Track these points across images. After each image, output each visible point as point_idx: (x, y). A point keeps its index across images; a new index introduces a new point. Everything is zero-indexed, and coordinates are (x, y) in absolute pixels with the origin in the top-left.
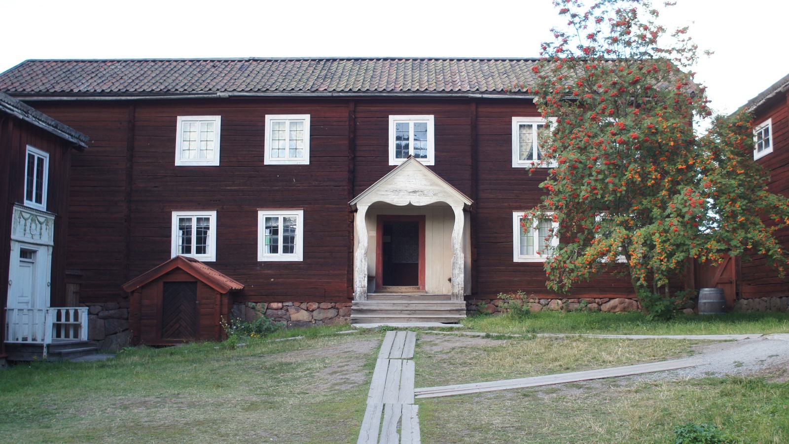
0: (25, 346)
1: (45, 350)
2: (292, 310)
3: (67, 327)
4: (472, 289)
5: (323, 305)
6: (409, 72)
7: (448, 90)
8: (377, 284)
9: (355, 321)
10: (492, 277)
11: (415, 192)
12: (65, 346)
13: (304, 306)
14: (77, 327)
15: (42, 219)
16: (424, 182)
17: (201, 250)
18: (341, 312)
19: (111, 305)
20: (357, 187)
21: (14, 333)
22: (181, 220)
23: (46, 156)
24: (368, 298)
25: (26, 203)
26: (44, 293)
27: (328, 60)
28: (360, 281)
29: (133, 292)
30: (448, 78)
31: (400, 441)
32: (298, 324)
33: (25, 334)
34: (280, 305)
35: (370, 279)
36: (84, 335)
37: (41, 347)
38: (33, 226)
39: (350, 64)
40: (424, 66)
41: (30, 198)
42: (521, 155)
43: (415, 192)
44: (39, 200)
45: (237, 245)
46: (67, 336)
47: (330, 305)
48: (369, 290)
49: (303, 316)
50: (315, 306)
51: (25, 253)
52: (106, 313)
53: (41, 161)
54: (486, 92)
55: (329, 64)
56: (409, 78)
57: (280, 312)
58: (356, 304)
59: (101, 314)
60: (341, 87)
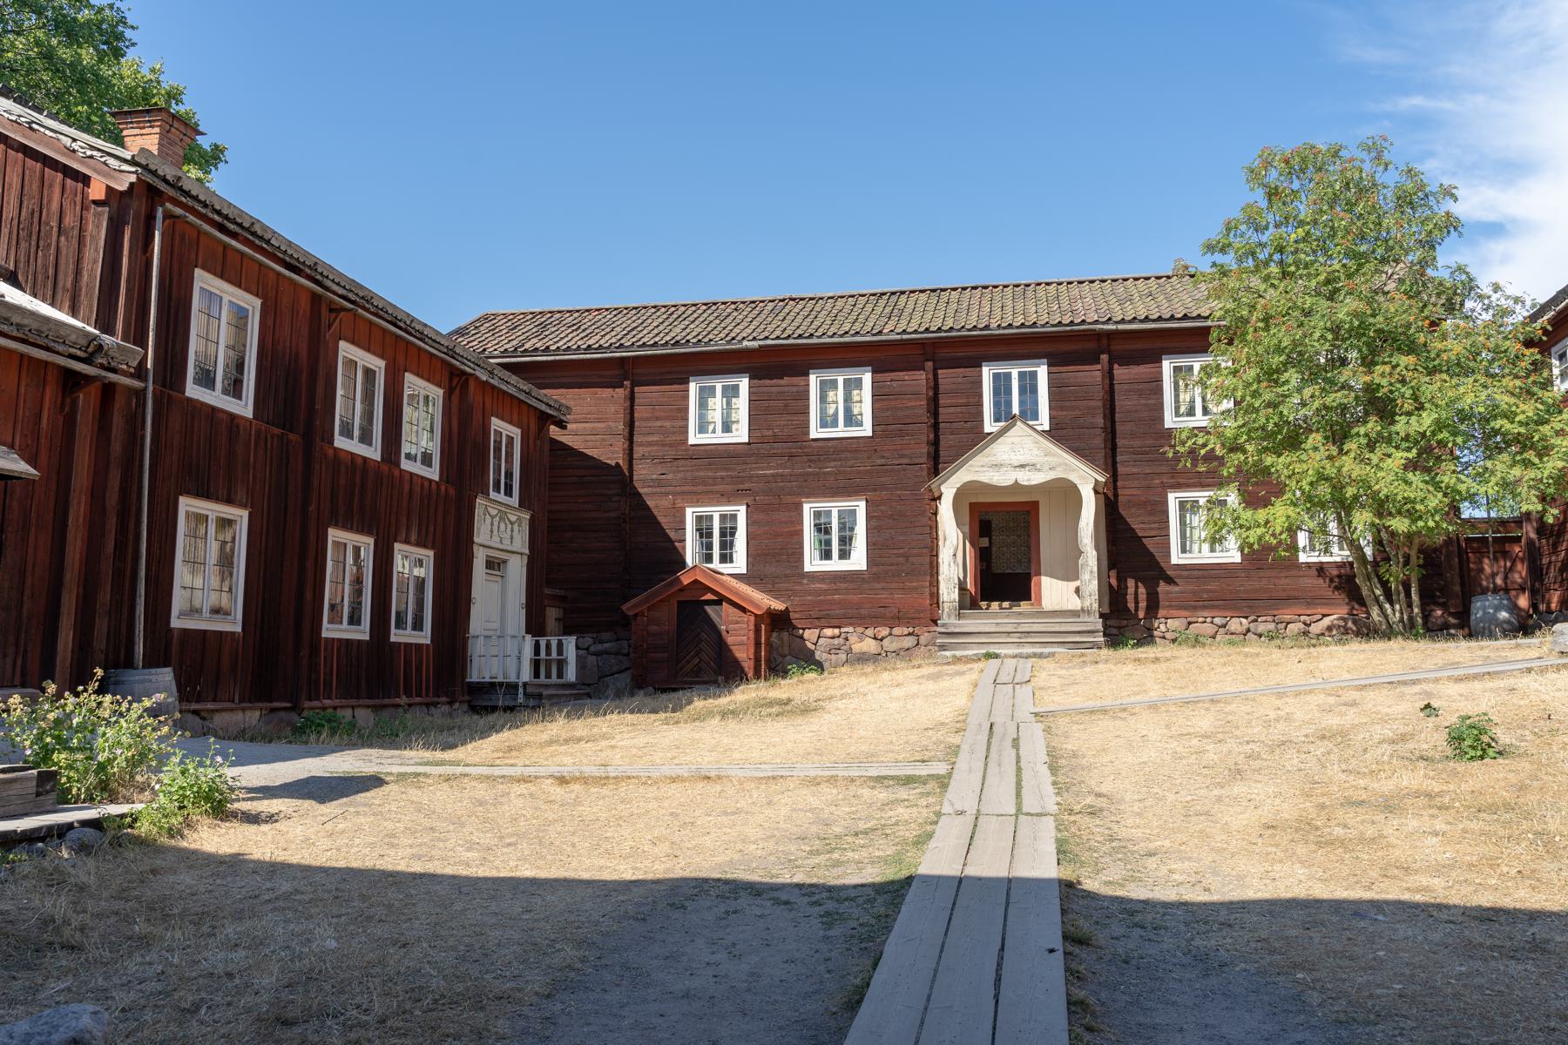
0: (492, 686)
1: (521, 690)
2: (853, 639)
3: (548, 663)
4: (1111, 604)
5: (896, 631)
6: (1009, 303)
7: (1066, 320)
8: (969, 603)
9: (943, 647)
10: (1132, 560)
11: (1022, 466)
12: (547, 686)
13: (870, 632)
14: (561, 664)
15: (513, 518)
16: (1035, 452)
17: (726, 558)
18: (923, 640)
19: (605, 636)
20: (936, 465)
21: (480, 671)
22: (699, 519)
23: (516, 432)
24: (959, 616)
25: (493, 495)
26: (516, 616)
27: (893, 293)
28: (949, 593)
29: (636, 615)
30: (1065, 306)
31: (632, 398)
32: (863, 658)
33: (494, 672)
34: (836, 631)
35: (962, 588)
36: (571, 674)
37: (515, 686)
38: (502, 526)
39: (923, 297)
40: (1030, 293)
41: (497, 489)
42: (1177, 408)
43: (1022, 466)
44: (509, 492)
45: (775, 553)
46: (548, 676)
47: (906, 631)
48: (962, 607)
49: (869, 645)
50: (884, 631)
51: (491, 564)
52: (600, 647)
53: (510, 440)
54: (1123, 321)
55: (894, 298)
56: (1009, 309)
57: (836, 641)
58: (943, 625)
59: (592, 649)
60: (913, 326)
